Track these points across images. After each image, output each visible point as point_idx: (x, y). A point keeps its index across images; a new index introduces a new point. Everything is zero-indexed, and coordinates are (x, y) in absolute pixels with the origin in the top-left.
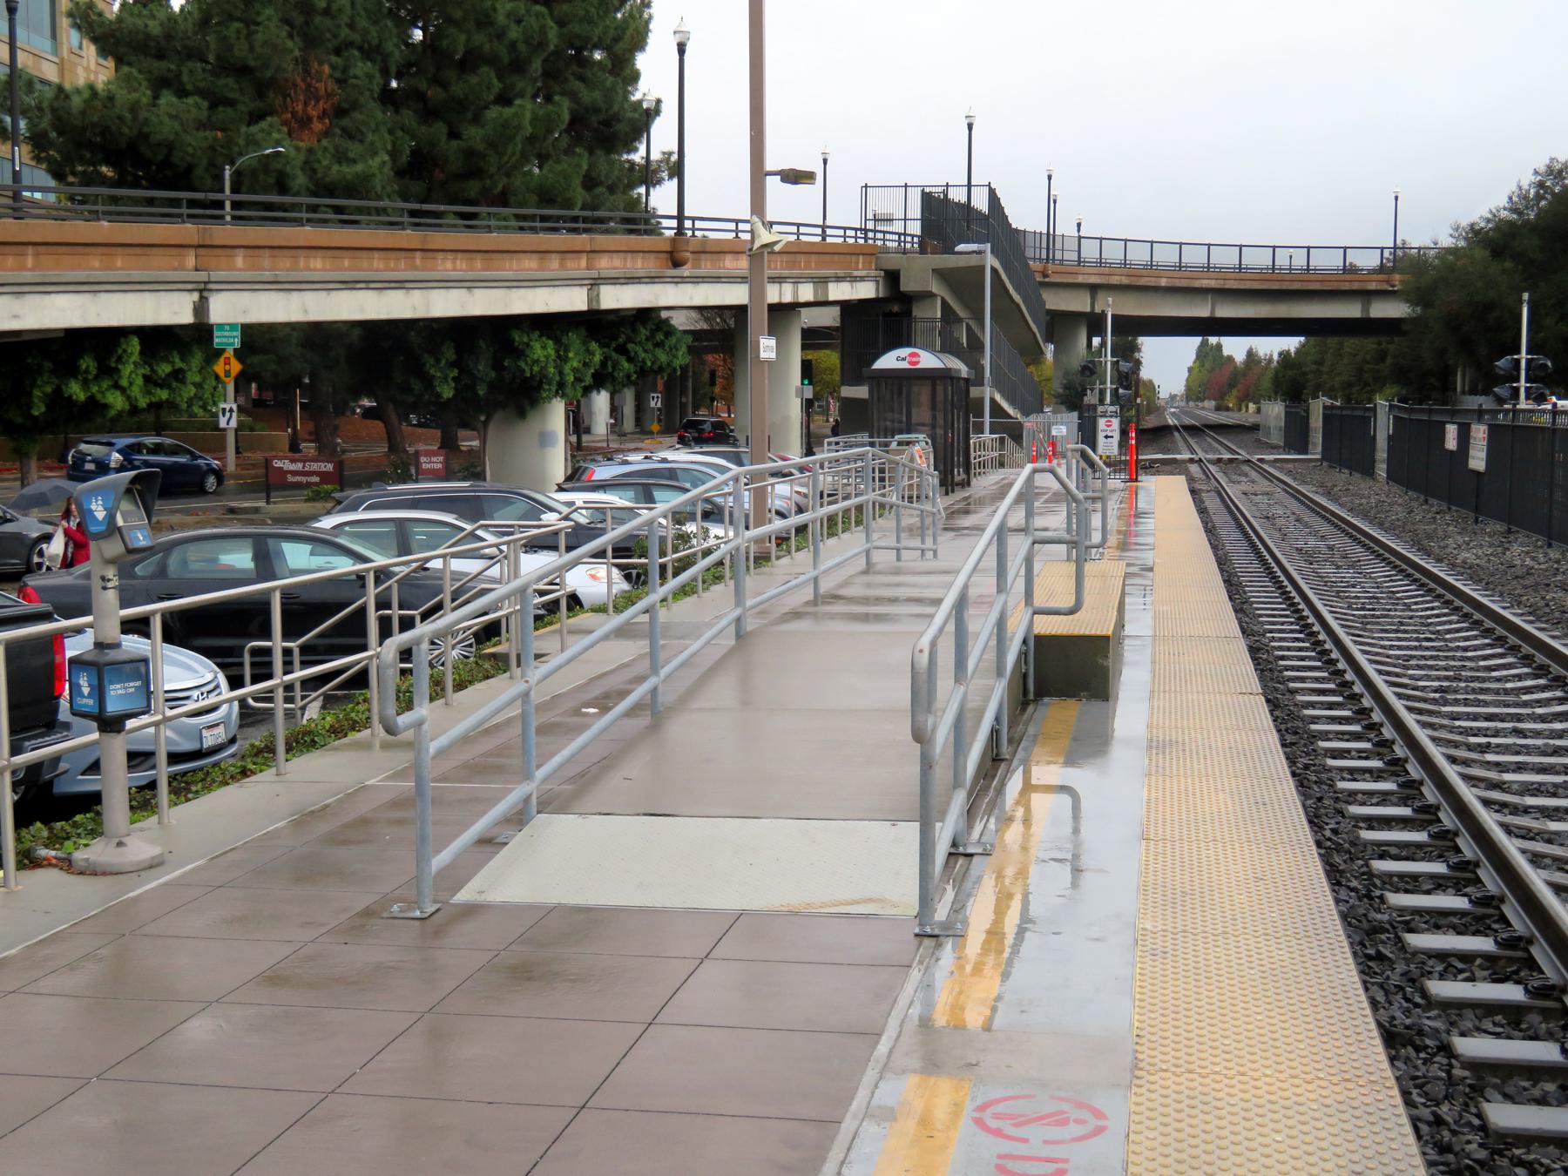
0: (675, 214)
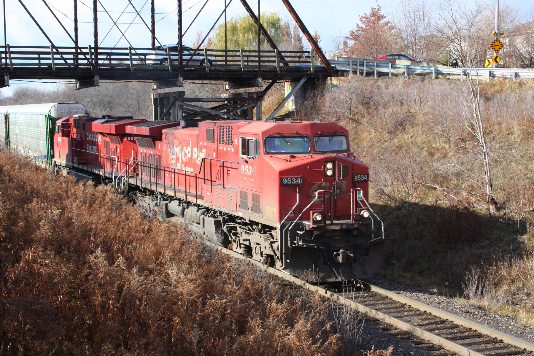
0: (227, 49)
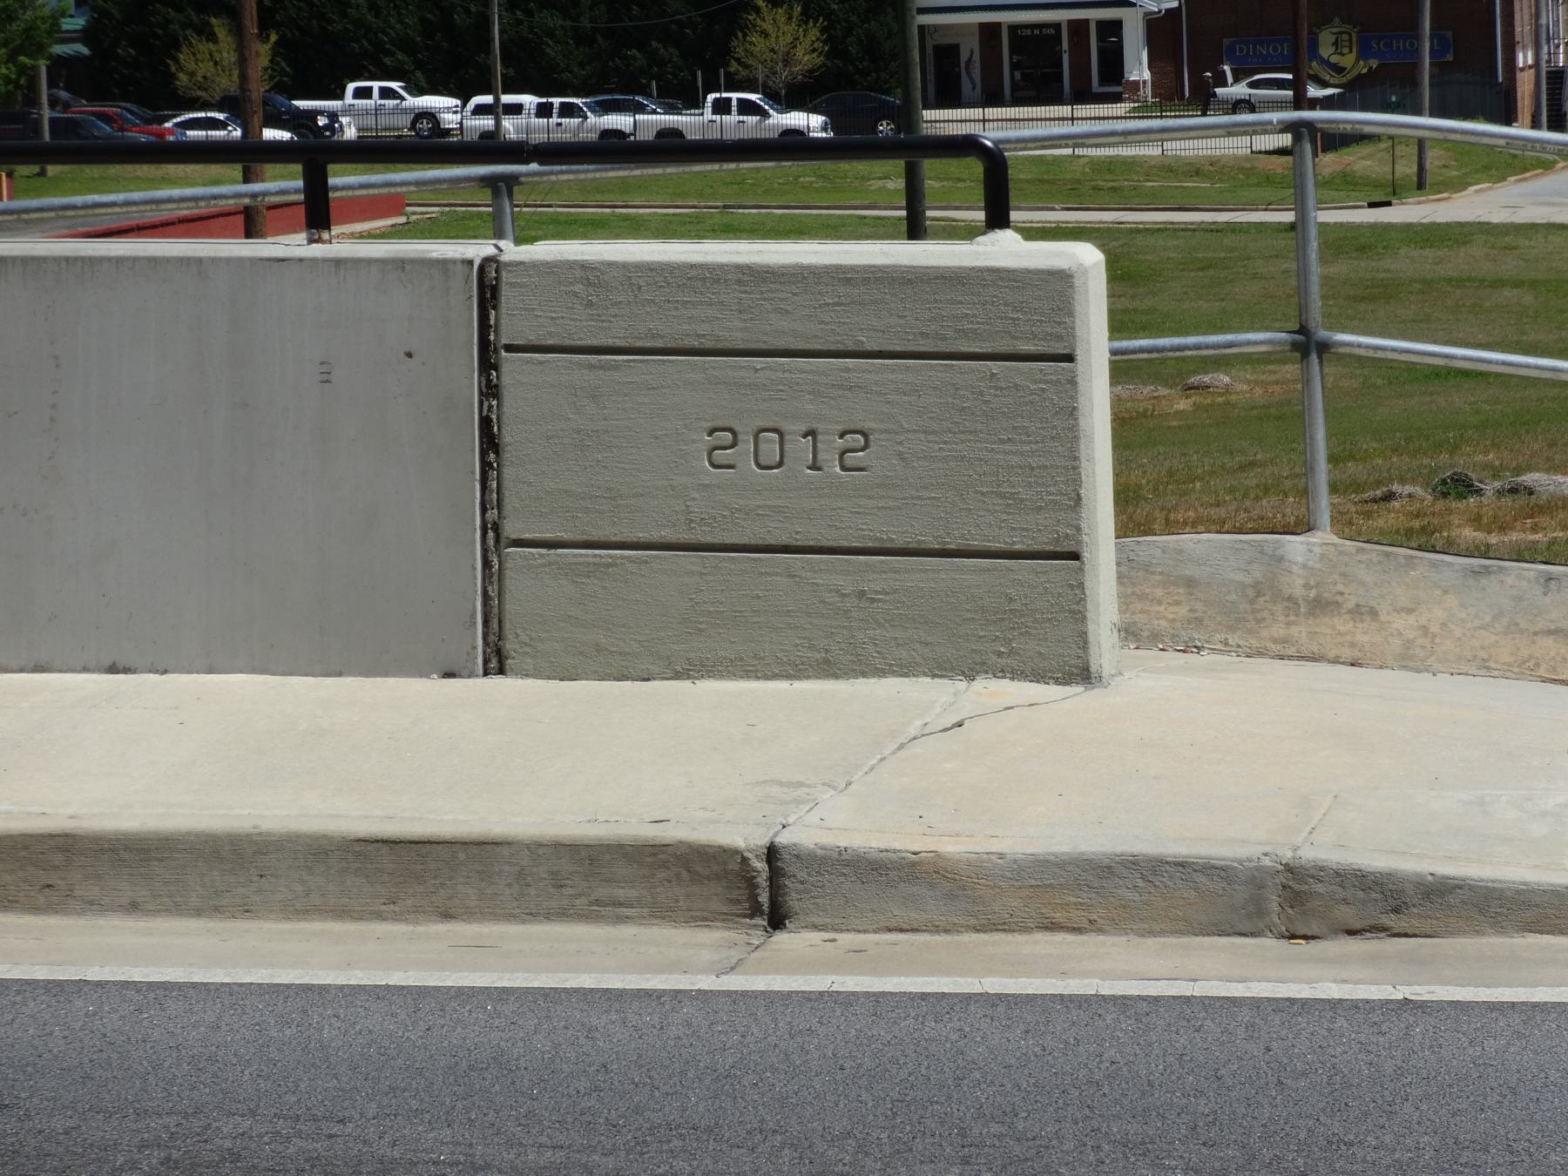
0: (899, 165)
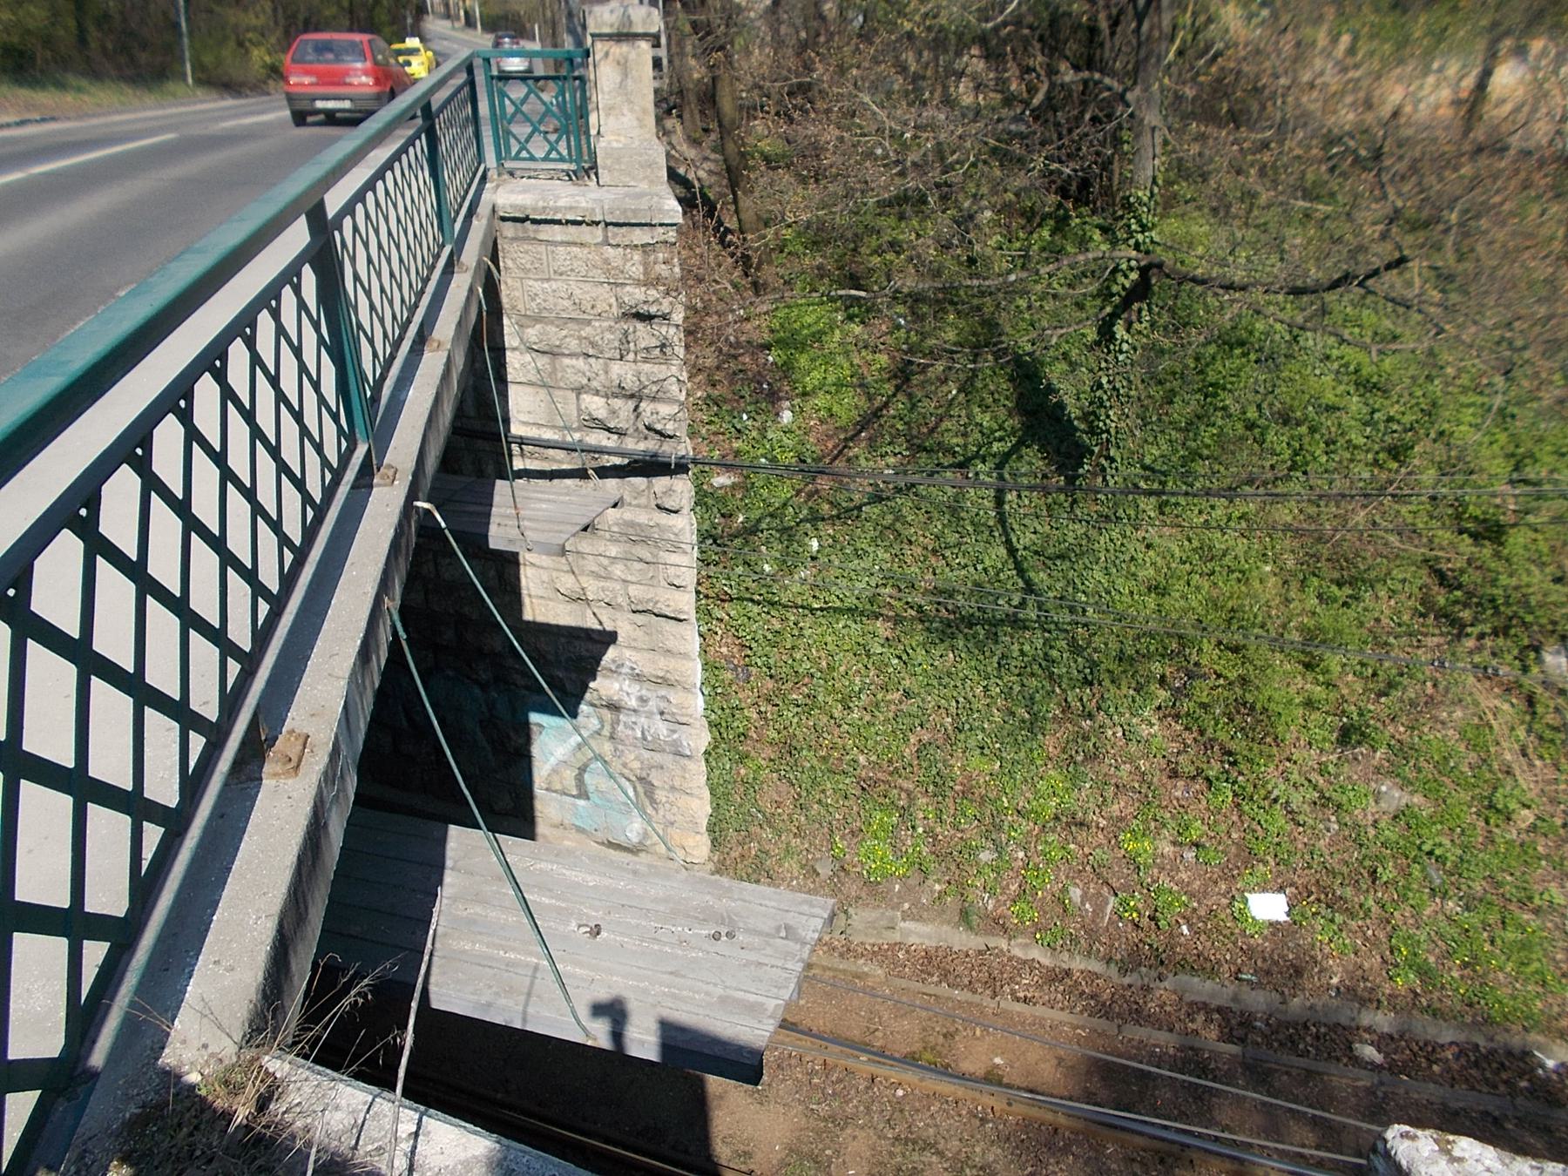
0: (62, 943)
